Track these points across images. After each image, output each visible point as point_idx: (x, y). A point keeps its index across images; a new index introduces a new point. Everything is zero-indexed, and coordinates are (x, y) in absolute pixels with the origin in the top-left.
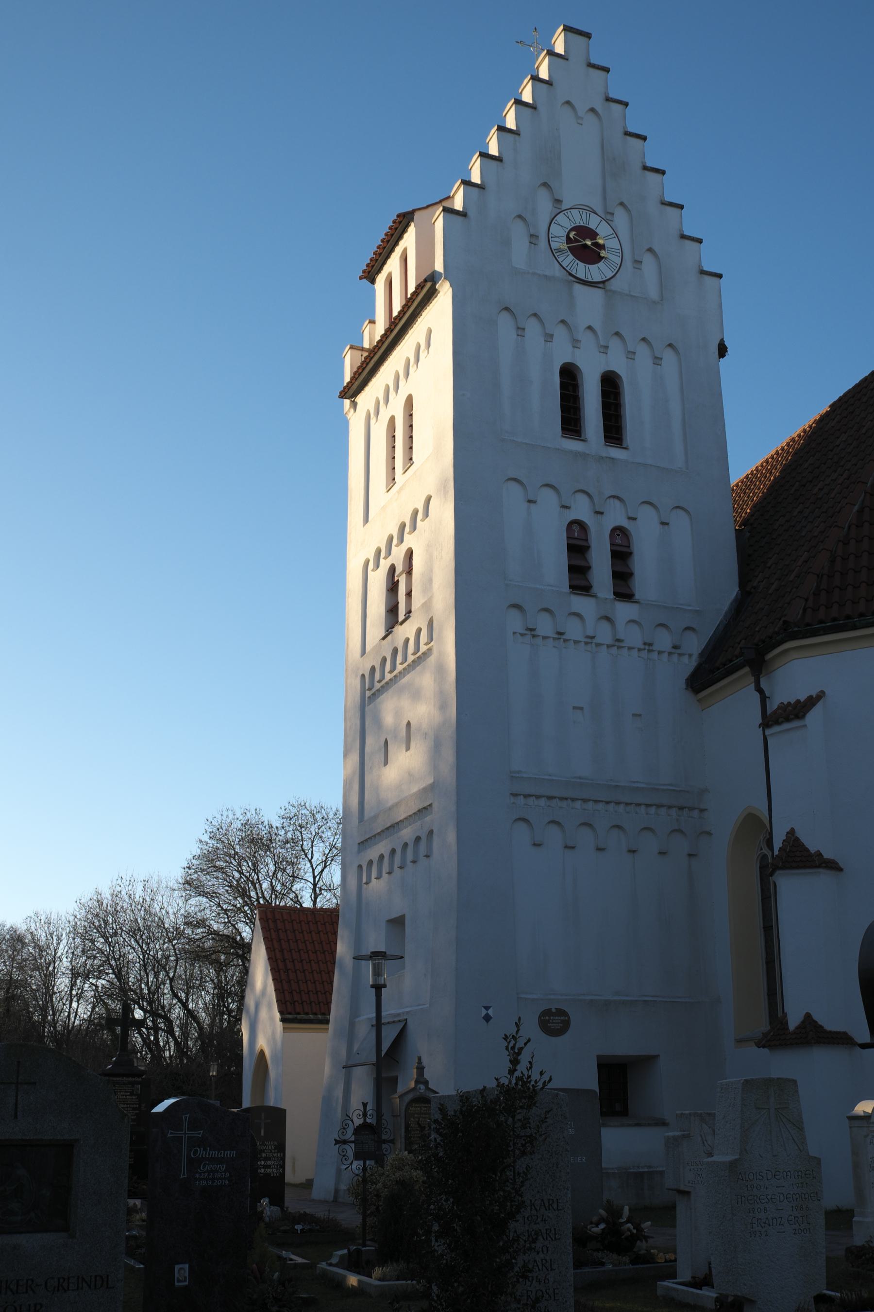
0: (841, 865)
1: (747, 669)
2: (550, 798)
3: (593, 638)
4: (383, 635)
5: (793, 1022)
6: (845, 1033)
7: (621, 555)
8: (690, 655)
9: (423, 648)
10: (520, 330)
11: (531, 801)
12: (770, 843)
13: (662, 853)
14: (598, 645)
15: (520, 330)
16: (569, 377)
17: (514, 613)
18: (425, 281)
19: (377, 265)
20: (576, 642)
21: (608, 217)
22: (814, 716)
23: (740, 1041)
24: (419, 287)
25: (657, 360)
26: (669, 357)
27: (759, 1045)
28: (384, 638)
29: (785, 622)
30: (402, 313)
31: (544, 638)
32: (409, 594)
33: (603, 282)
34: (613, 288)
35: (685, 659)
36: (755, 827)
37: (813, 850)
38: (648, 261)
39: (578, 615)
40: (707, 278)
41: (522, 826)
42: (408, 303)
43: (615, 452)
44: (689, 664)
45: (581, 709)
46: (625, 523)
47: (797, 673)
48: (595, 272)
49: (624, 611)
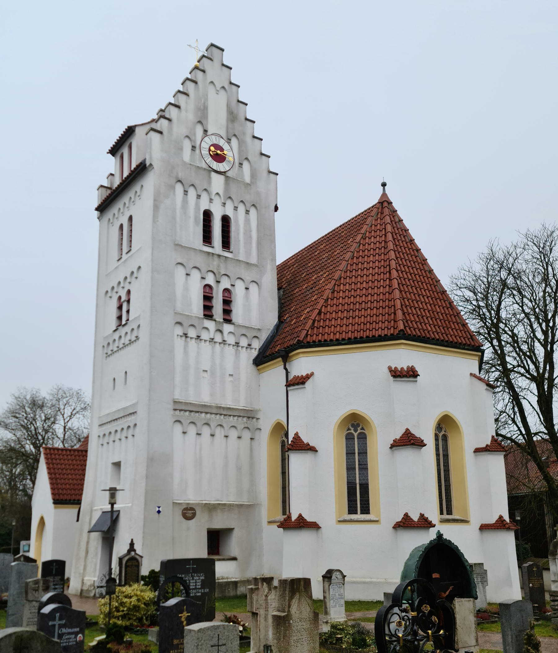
0: (317, 449)
1: (280, 359)
2: (191, 411)
3: (213, 339)
4: (115, 328)
5: (294, 517)
6: (315, 522)
8: (255, 349)
10: (186, 192)
11: (182, 412)
12: (287, 435)
13: (239, 437)
14: (215, 342)
15: (186, 192)
16: (207, 215)
17: (178, 326)
20: (205, 341)
21: (229, 141)
23: (270, 522)
24: (138, 166)
25: (247, 212)
26: (253, 211)
28: (115, 331)
31: (191, 338)
33: (225, 172)
34: (229, 175)
35: (253, 351)
36: (280, 430)
37: (305, 442)
38: (246, 165)
39: (207, 328)
40: (271, 175)
41: (178, 424)
44: (255, 353)
45: (206, 371)
46: (229, 287)
47: (302, 364)
48: (221, 167)
49: (227, 328)
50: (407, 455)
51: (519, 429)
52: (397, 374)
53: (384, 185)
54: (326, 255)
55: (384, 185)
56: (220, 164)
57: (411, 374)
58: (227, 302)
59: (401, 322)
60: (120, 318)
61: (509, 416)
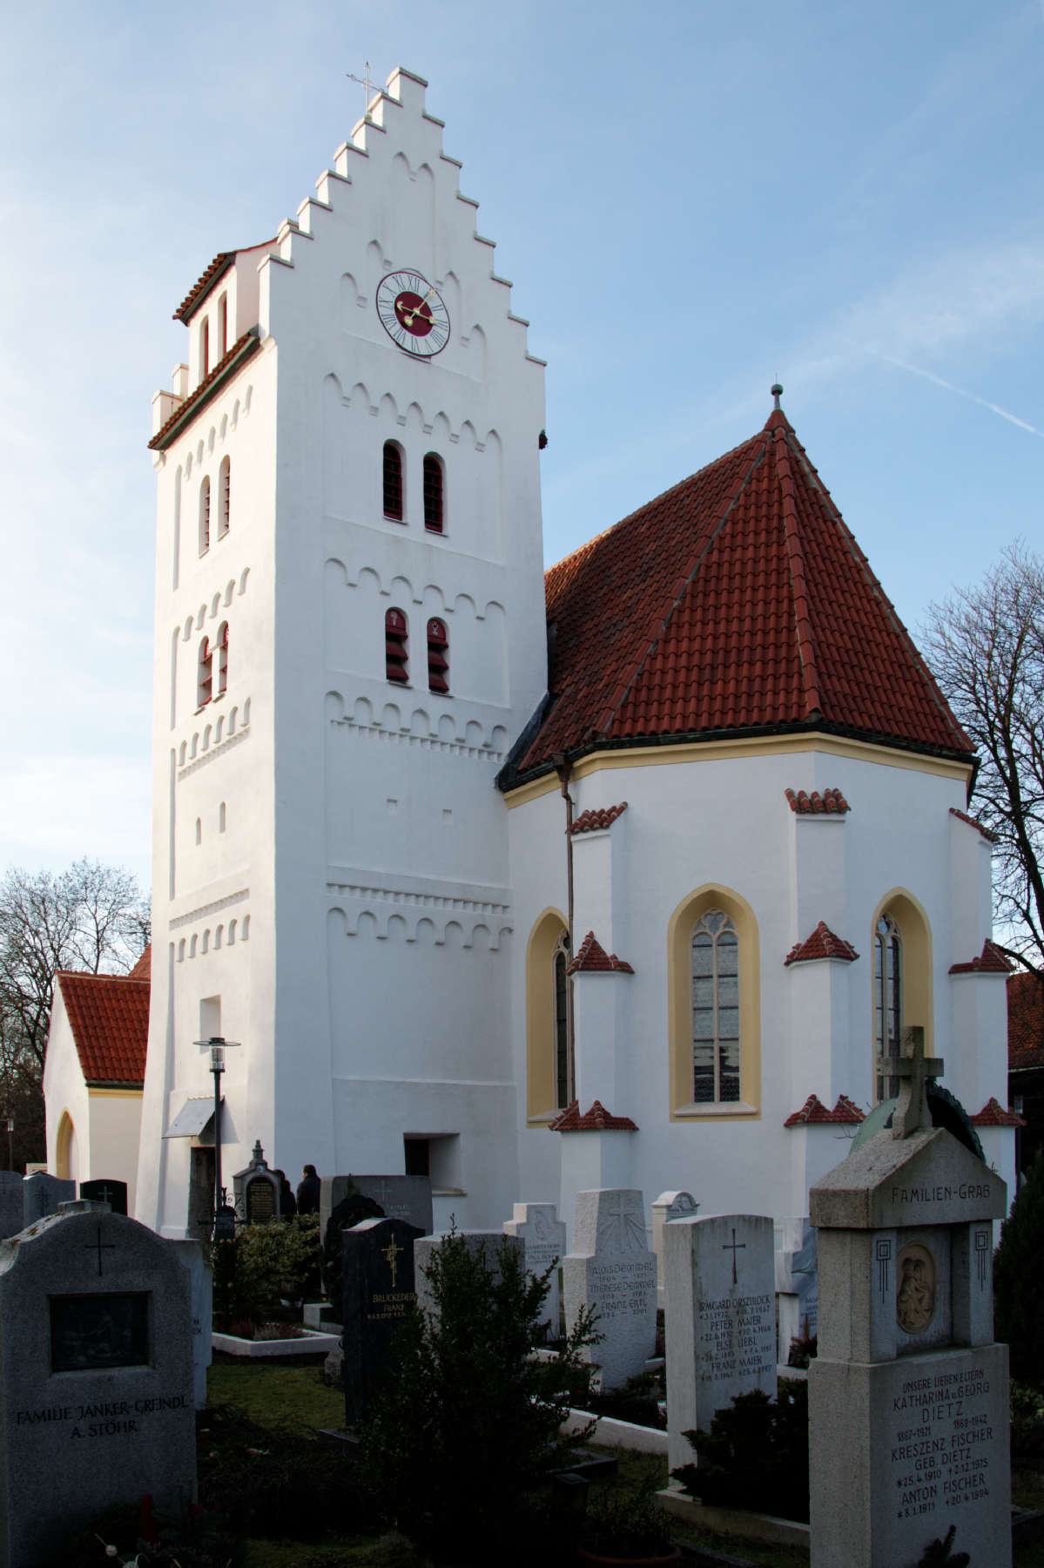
0: (634, 967)
1: (555, 774)
5: (584, 1109)
7: (438, 645)
9: (239, 729)
12: (567, 941)
16: (392, 454)
18: (249, 335)
19: (193, 306)
20: (392, 734)
22: (617, 825)
23: (531, 1123)
24: (242, 341)
27: (551, 1128)
29: (594, 732)
30: (218, 370)
32: (224, 670)
36: (555, 929)
42: (227, 357)
43: (432, 539)
47: (600, 783)
50: (821, 973)
51: (1035, 935)
52: (804, 805)
53: (777, 391)
54: (653, 546)
55: (777, 391)
56: (420, 339)
57: (828, 805)
58: (438, 645)
59: (814, 693)
60: (206, 685)
61: (1018, 905)
